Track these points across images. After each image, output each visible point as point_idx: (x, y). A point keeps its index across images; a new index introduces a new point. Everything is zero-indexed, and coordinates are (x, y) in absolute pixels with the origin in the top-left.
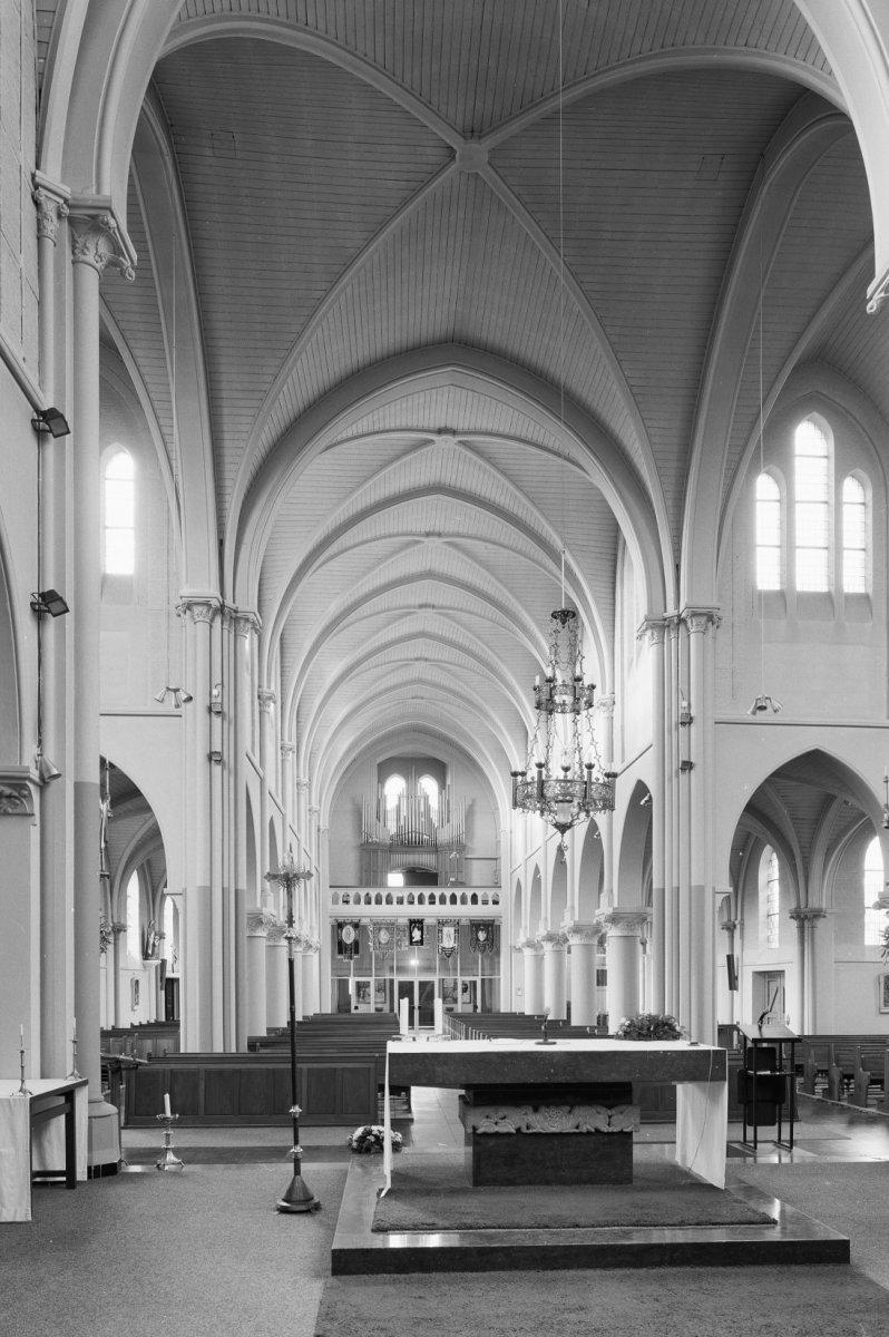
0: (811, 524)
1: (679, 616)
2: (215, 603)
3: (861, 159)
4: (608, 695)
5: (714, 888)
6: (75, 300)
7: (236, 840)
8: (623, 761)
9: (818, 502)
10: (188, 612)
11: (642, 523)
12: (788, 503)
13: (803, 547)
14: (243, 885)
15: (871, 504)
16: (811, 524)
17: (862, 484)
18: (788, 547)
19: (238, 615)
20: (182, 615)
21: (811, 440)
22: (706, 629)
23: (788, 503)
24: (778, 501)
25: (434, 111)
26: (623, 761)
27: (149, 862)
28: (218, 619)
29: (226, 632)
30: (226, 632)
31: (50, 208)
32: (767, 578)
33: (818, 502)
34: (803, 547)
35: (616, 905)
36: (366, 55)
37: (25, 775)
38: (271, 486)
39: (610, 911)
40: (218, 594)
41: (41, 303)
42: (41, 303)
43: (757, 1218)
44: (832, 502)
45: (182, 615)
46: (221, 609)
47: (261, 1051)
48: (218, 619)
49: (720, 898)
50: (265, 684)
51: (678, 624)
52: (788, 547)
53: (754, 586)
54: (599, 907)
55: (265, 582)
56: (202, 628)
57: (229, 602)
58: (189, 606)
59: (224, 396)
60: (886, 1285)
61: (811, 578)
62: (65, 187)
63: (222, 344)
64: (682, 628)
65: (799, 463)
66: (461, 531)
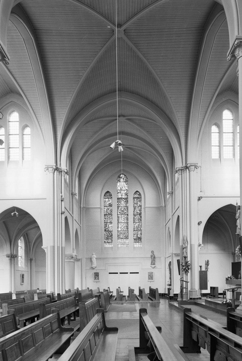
3: (228, 32)
4: (170, 190)
9: (26, 135)
12: (220, 133)
13: (16, 122)
14: (63, 246)
19: (62, 170)
20: (46, 171)
22: (194, 170)
23: (220, 133)
24: (218, 133)
25: (112, 23)
27: (27, 234)
28: (56, 171)
29: (58, 175)
34: (16, 122)
36: (94, 8)
40: (55, 165)
43: (11, 239)
45: (46, 171)
48: (56, 171)
50: (73, 190)
51: (186, 169)
57: (58, 166)
64: (187, 170)
65: (224, 122)
66: (128, 144)
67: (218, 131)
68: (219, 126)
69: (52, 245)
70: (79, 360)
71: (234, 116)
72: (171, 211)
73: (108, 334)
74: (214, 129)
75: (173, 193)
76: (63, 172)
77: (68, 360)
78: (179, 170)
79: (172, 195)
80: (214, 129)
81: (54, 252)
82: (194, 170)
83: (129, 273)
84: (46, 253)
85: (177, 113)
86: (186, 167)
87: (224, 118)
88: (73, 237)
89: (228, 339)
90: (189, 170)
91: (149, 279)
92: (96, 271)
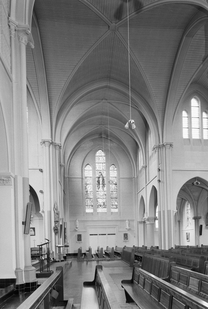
0: (195, 123)
1: (163, 145)
2: (51, 142)
5: (173, 211)
6: (15, 218)
7: (57, 196)
8: (149, 181)
9: (197, 118)
10: (44, 144)
11: (155, 126)
12: (190, 117)
15: (200, 107)
16: (195, 123)
17: (197, 100)
18: (190, 128)
20: (42, 145)
21: (195, 103)
22: (170, 148)
23: (190, 117)
26: (149, 181)
28: (51, 146)
29: (53, 149)
30: (53, 149)
31: (13, 27)
32: (185, 135)
33: (197, 118)
35: (148, 216)
37: (10, 175)
38: (62, 116)
39: (147, 217)
41: (11, 55)
42: (11, 55)
44: (200, 117)
45: (42, 145)
46: (52, 143)
47: (59, 210)
48: (51, 146)
49: (174, 213)
52: (190, 128)
53: (182, 137)
54: (144, 217)
55: (65, 155)
56: (47, 148)
57: (53, 141)
58: (44, 142)
59: (53, 108)
60: (207, 289)
61: (196, 135)
62: (16, 22)
63: (52, 88)
67: (187, 116)
68: (189, 112)
69: (49, 210)
70: (36, 308)
71: (200, 103)
72: (145, 182)
73: (92, 287)
74: (184, 114)
75: (146, 167)
76: (57, 146)
77: (29, 308)
78: (156, 147)
79: (146, 168)
80: (184, 114)
81: (161, 225)
82: (170, 148)
83: (107, 235)
84: (44, 217)
85: (155, 98)
86: (163, 145)
87: (192, 105)
88: (147, 209)
89: (196, 294)
90: (165, 148)
91: (124, 239)
92: (79, 234)
